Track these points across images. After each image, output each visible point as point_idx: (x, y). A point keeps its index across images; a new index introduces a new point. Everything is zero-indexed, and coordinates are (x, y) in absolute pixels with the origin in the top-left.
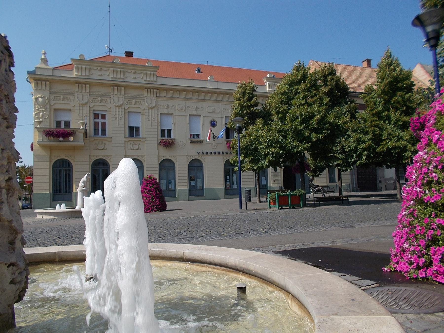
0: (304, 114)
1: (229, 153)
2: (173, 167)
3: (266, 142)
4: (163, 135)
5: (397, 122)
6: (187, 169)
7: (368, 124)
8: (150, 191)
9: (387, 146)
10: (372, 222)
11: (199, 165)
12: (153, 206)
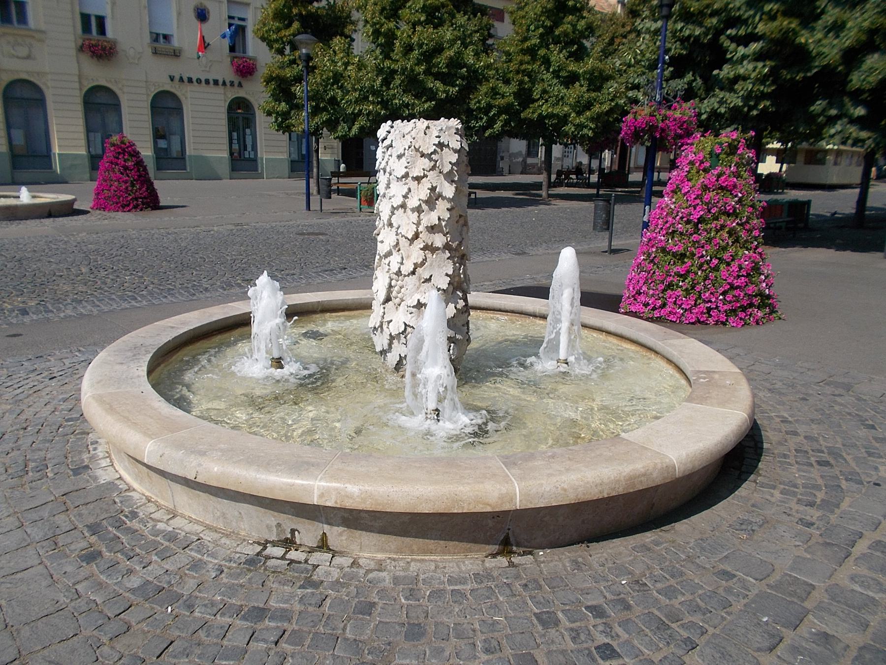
1: (236, 84)
2: (116, 106)
3: (356, 90)
4: (86, 28)
5: (559, 71)
6: (148, 111)
7: (513, 66)
8: (126, 168)
10: (544, 245)
11: (171, 104)
12: (136, 199)
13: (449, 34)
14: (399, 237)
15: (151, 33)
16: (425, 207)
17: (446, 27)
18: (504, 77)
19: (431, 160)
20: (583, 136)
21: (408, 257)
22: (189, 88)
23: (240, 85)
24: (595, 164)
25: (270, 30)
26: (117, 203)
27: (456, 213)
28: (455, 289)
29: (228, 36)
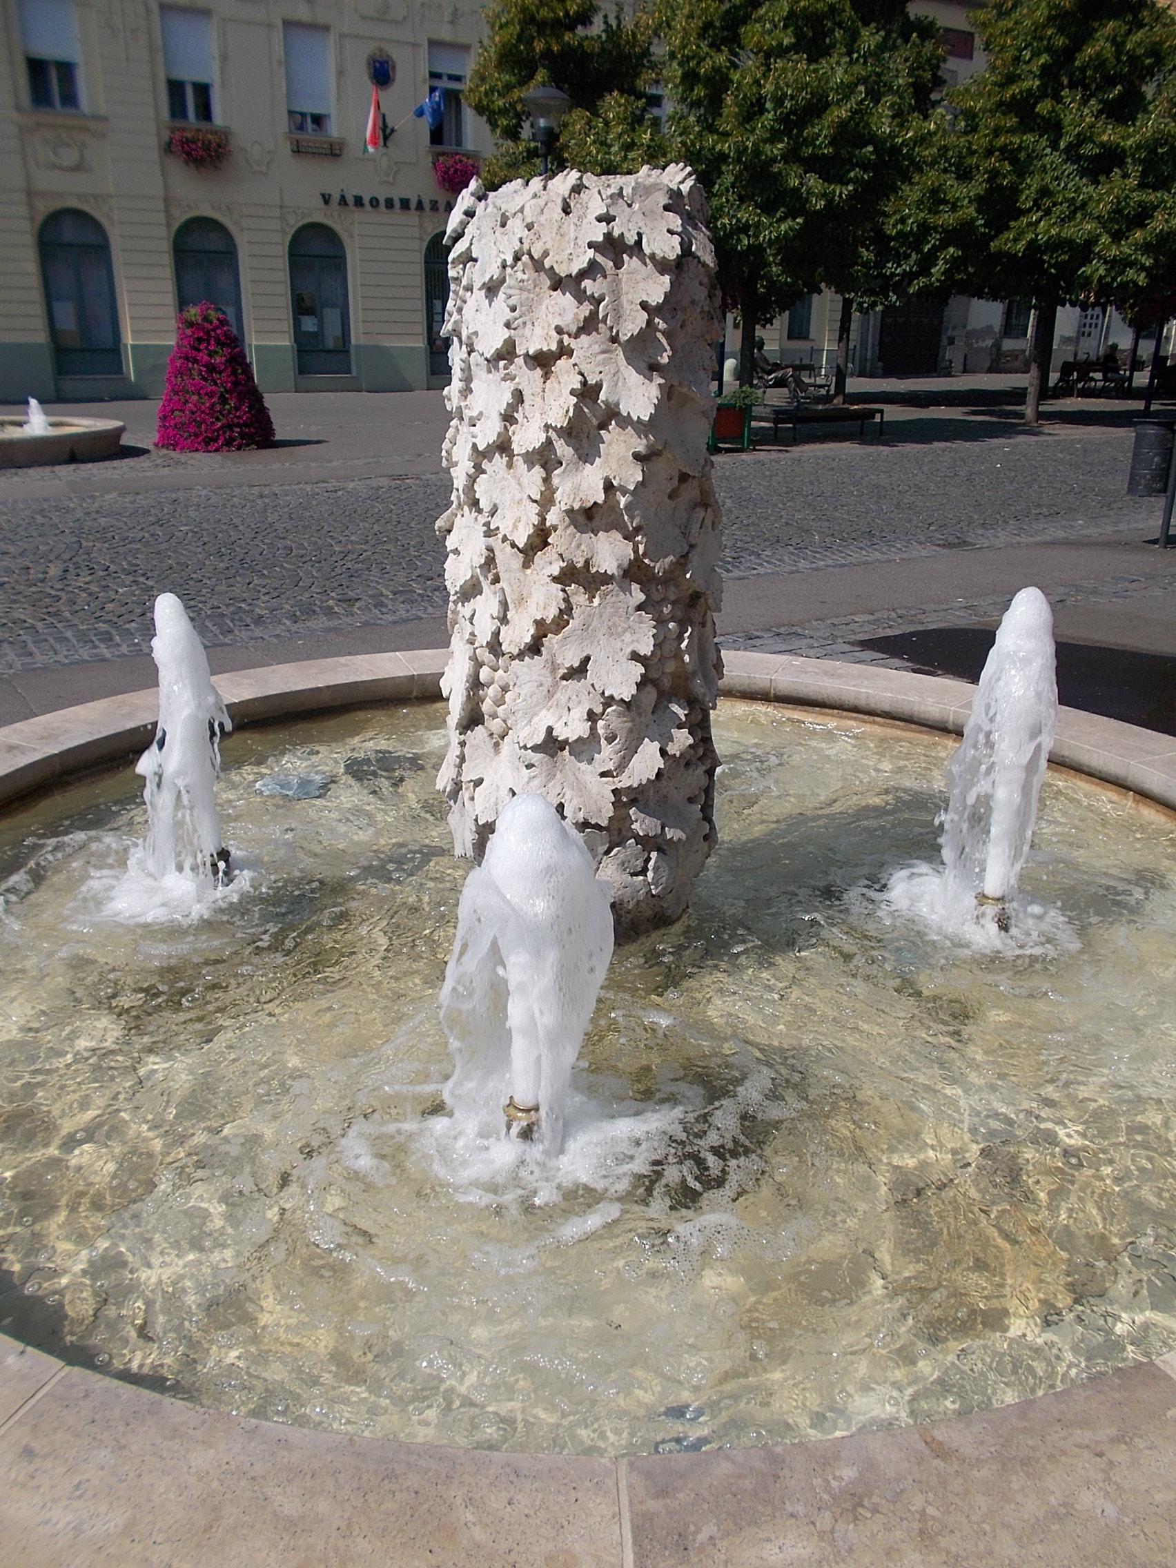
0: (792, 97)
2: (229, 255)
4: (178, 109)
6: (283, 263)
7: (980, 140)
8: (212, 368)
9: (1031, 236)
12: (229, 427)
13: (840, 72)
14: (495, 542)
15: (290, 113)
16: (563, 449)
17: (833, 61)
18: (958, 166)
19: (580, 296)
20: (1123, 285)
21: (522, 600)
22: (357, 216)
24: (1146, 349)
25: (492, 89)
26: (196, 436)
27: (665, 469)
28: (665, 697)
29: (428, 111)
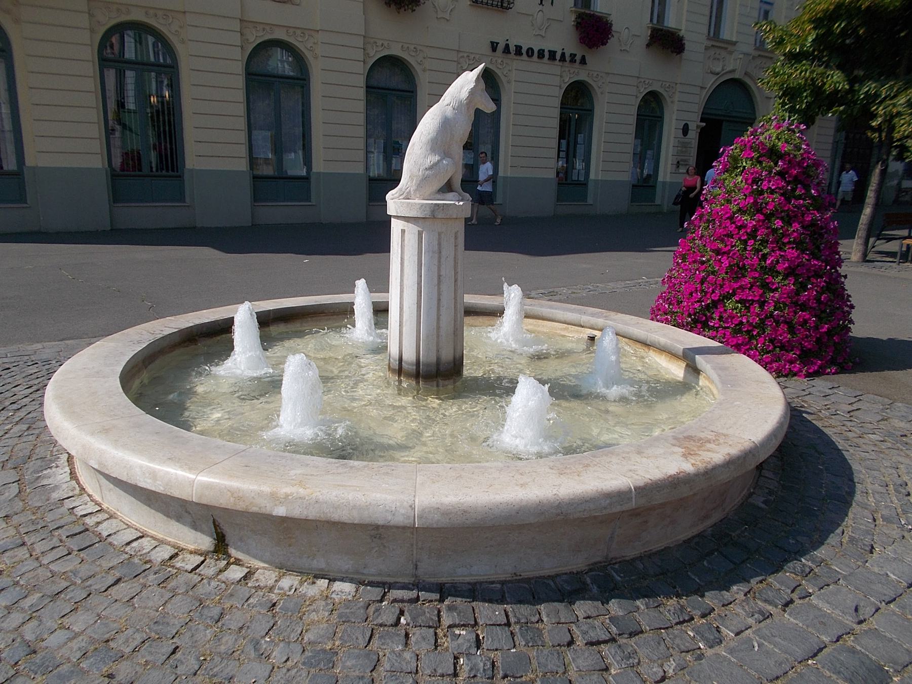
1: (578, 58)
23: (583, 61)
